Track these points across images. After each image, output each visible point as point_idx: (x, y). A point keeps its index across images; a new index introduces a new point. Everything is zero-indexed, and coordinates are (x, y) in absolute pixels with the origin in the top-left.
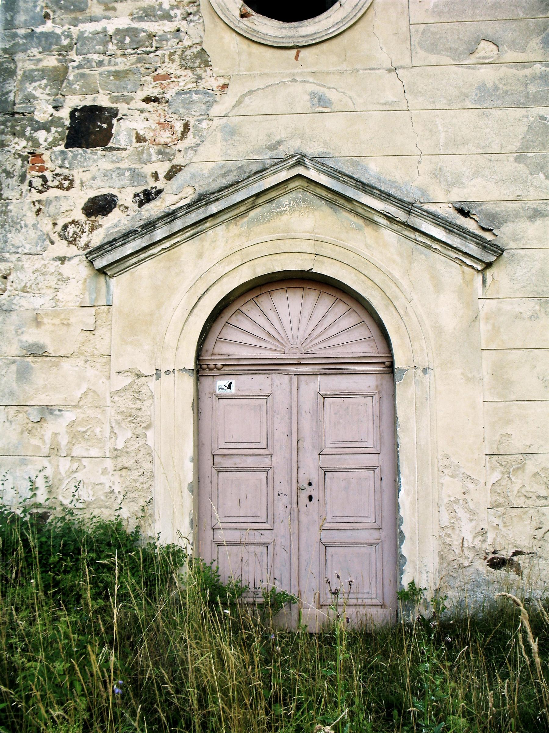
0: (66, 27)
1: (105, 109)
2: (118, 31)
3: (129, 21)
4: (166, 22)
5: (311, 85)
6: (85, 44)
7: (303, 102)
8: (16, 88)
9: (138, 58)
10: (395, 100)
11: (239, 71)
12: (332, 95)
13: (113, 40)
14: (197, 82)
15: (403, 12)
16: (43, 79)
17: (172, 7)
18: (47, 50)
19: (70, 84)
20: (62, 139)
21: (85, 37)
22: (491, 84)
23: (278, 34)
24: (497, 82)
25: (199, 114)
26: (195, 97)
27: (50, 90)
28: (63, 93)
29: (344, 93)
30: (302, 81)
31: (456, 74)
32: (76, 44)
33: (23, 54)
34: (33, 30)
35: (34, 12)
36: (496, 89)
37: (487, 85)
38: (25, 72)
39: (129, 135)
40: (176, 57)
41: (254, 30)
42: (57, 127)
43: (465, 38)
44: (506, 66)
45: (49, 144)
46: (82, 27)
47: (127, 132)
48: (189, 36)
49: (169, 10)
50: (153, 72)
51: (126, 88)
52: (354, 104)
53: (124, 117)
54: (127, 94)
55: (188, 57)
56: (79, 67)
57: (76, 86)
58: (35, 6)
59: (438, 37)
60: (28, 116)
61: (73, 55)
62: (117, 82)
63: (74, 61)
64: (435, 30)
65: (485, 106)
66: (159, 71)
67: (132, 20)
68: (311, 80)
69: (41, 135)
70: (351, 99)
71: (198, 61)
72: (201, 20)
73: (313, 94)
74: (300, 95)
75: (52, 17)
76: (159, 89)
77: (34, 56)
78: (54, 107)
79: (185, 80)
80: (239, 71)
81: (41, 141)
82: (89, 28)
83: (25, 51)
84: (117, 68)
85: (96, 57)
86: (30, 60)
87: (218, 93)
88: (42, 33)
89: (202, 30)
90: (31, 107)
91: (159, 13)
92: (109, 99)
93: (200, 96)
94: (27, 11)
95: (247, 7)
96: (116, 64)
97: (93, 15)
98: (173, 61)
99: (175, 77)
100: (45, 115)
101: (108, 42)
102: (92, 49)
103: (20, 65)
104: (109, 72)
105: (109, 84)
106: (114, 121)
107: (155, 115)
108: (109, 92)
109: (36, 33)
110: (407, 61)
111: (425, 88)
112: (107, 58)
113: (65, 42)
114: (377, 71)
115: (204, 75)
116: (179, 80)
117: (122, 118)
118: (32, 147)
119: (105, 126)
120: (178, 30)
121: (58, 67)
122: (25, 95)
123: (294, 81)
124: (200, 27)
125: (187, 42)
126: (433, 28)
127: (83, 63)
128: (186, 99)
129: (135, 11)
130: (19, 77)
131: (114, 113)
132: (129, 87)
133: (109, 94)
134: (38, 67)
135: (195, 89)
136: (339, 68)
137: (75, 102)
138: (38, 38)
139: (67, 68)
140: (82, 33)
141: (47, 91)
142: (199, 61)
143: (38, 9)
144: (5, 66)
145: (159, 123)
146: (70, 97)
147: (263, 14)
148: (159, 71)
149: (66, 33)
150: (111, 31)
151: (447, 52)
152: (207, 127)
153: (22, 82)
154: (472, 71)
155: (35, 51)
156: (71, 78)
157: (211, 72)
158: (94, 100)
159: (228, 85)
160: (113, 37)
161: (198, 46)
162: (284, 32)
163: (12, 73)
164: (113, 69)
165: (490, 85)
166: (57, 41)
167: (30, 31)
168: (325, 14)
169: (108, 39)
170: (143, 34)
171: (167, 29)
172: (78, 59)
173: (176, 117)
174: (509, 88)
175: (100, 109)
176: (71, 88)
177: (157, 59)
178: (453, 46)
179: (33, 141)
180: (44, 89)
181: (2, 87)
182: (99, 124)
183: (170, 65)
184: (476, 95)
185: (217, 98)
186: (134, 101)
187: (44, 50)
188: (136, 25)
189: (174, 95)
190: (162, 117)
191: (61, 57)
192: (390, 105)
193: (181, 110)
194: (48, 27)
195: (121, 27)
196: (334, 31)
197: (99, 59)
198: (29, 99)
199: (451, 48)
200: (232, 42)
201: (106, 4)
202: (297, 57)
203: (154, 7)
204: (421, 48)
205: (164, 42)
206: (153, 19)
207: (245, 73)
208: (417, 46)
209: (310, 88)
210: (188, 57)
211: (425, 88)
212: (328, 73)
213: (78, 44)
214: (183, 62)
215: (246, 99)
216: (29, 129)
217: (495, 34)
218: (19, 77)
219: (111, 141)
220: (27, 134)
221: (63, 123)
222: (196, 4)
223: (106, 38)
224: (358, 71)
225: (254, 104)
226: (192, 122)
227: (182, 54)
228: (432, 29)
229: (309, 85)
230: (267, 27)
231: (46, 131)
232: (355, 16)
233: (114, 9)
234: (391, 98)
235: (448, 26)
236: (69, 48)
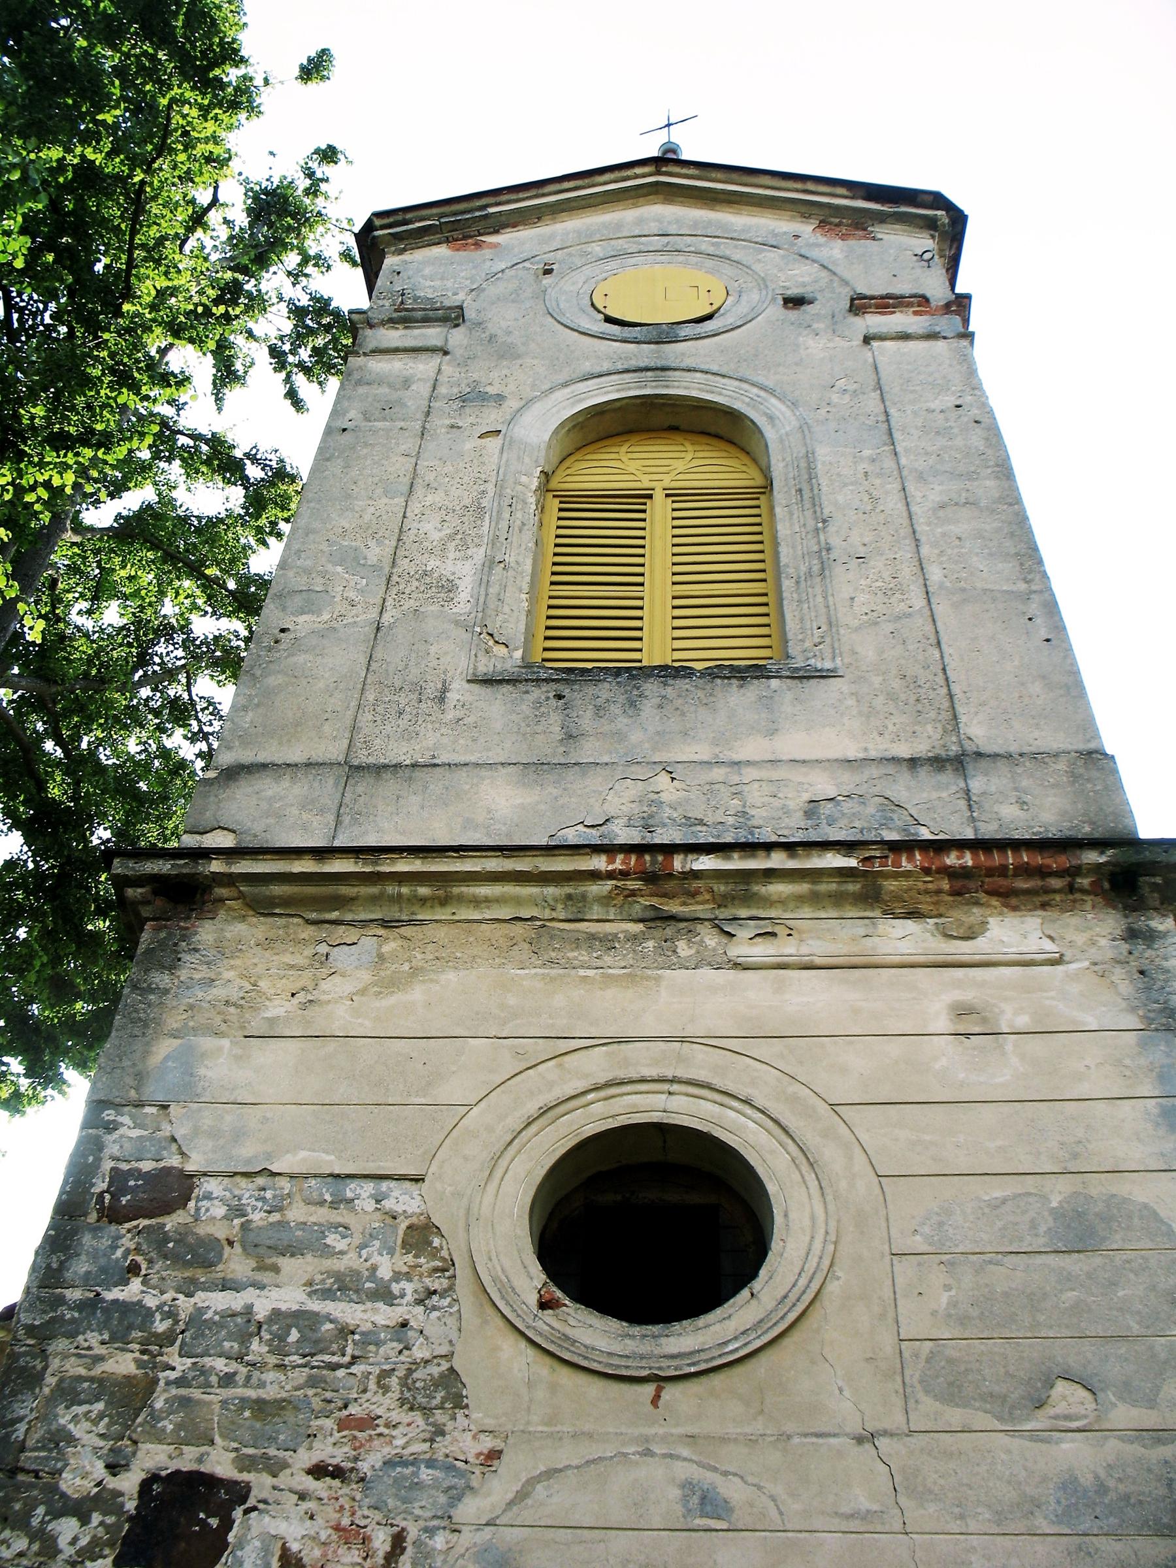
0: (168, 1296)
1: (221, 1480)
2: (276, 1314)
3: (303, 1297)
4: (380, 1305)
5: (685, 1464)
6: (203, 1335)
7: (667, 1501)
8: (34, 1415)
9: (310, 1377)
10: (875, 1507)
11: (528, 1423)
12: (732, 1491)
13: (262, 1334)
14: (432, 1441)
15: (882, 1316)
16: (98, 1400)
17: (397, 1276)
18: (119, 1339)
19: (155, 1417)
20: (111, 1544)
21: (206, 1321)
22: (1090, 1477)
23: (616, 1348)
24: (1102, 1474)
25: (429, 1514)
26: (425, 1474)
27: (108, 1426)
28: (134, 1436)
29: (759, 1488)
30: (665, 1456)
31: (1009, 1452)
32: (182, 1332)
33: (67, 1342)
34: (98, 1294)
35: (109, 1258)
36: (1102, 1489)
37: (1082, 1480)
38: (61, 1380)
39: (266, 1551)
40: (394, 1381)
41: (566, 1337)
42: (105, 1514)
43: (1022, 1374)
44: (1119, 1438)
45: (78, 1553)
46: (201, 1298)
47: (263, 1542)
48: (427, 1339)
49: (390, 1281)
50: (340, 1410)
51: (276, 1439)
52: (781, 1514)
53: (261, 1506)
54: (276, 1453)
55: (419, 1384)
56: (181, 1382)
57: (165, 1423)
58: (114, 1248)
59: (963, 1369)
60: (47, 1479)
61: (171, 1355)
62: (258, 1425)
63: (173, 1369)
64: (955, 1354)
65: (1082, 1528)
66: (353, 1409)
67: (310, 1295)
68: (685, 1452)
69: (67, 1529)
70: (774, 1500)
71: (440, 1395)
72: (455, 1308)
73: (688, 1486)
74: (661, 1485)
75: (143, 1272)
76: (346, 1449)
77: (89, 1348)
78: (107, 1467)
79: (407, 1433)
80: (528, 1423)
81: (63, 1542)
82: (217, 1301)
83: (72, 1335)
84: (262, 1393)
85: (220, 1365)
86: (79, 1356)
87: (477, 1470)
88: (115, 1302)
89: (455, 1328)
90: (58, 1460)
91: (368, 1285)
92: (234, 1460)
93: (437, 1473)
94: (94, 1255)
95: (554, 1289)
96: (262, 1385)
97: (229, 1276)
98: (386, 1389)
99: (387, 1426)
100: (85, 1482)
101: (251, 1335)
102: (214, 1347)
103: (55, 1363)
104: (242, 1399)
105: (240, 1426)
106: (238, 1513)
107: (329, 1509)
108: (235, 1445)
109: (103, 1300)
110: (896, 1420)
111: (942, 1482)
112: (244, 1370)
113: (161, 1326)
114: (832, 1440)
115: (450, 1426)
116: (394, 1433)
117: (254, 1509)
118: (37, 1554)
119: (214, 1522)
120: (404, 1325)
121: (135, 1377)
122: (49, 1432)
123: (648, 1453)
124: (451, 1321)
125: (419, 1353)
126: (951, 1349)
127: (191, 1375)
128: (405, 1478)
129: (318, 1278)
130: (46, 1390)
131: (239, 1493)
132: (282, 1437)
133: (236, 1450)
134: (92, 1373)
135: (427, 1456)
136: (748, 1430)
137: (157, 1458)
138: (105, 1311)
139: (155, 1381)
140: (200, 1311)
141: (101, 1428)
142: (442, 1394)
143: (119, 1253)
144: (22, 1362)
145: (337, 1528)
146: (149, 1446)
147: (588, 1304)
148: (353, 1409)
149: (166, 1308)
150: (262, 1311)
151: (986, 1401)
152: (445, 1547)
153: (51, 1401)
154: (1044, 1447)
155: (92, 1339)
156: (159, 1405)
157: (467, 1422)
158: (200, 1460)
159: (501, 1452)
160: (265, 1327)
161: (443, 1362)
162: (630, 1346)
163: (34, 1379)
164: (252, 1393)
165: (1087, 1480)
166: (143, 1322)
167: (92, 1295)
168: (719, 1312)
169: (253, 1329)
170: (329, 1326)
171: (381, 1320)
172: (182, 1365)
173: (378, 1516)
174: (1132, 1488)
175: (211, 1481)
176: (153, 1426)
177: (352, 1381)
178: (997, 1388)
179: (43, 1541)
180: (95, 1422)
181: (4, 1407)
182: (202, 1515)
183: (379, 1398)
184: (1058, 1502)
185: (475, 1481)
186: (288, 1471)
187: (113, 1339)
188: (315, 1306)
189: (378, 1465)
190: (347, 1513)
191: (146, 1357)
192: (863, 1519)
193: (391, 1502)
194: (133, 1290)
195: (283, 1307)
196: (736, 1350)
197: (226, 1370)
198: (59, 1440)
199: (991, 1395)
200: (517, 1359)
201: (260, 1259)
202: (655, 1401)
203: (358, 1273)
204: (927, 1392)
205: (372, 1348)
206: (354, 1297)
207: (540, 1428)
208: (918, 1387)
209: (683, 1470)
210: (418, 1385)
211: (942, 1482)
212: (724, 1440)
213: (187, 1334)
214: (407, 1395)
215: (539, 1487)
216: (41, 1510)
217: (1085, 1367)
218: (46, 1390)
219: (223, 1560)
220: (35, 1522)
221: (122, 1505)
222: (447, 1274)
223: (246, 1326)
224: (789, 1437)
225: (554, 1501)
226: (413, 1532)
227: (407, 1376)
228: (950, 1352)
229: (680, 1463)
230: (595, 1333)
231: (79, 1520)
232: (782, 1318)
233: (276, 1269)
234: (865, 1504)
235: (983, 1347)
236: (168, 1339)
